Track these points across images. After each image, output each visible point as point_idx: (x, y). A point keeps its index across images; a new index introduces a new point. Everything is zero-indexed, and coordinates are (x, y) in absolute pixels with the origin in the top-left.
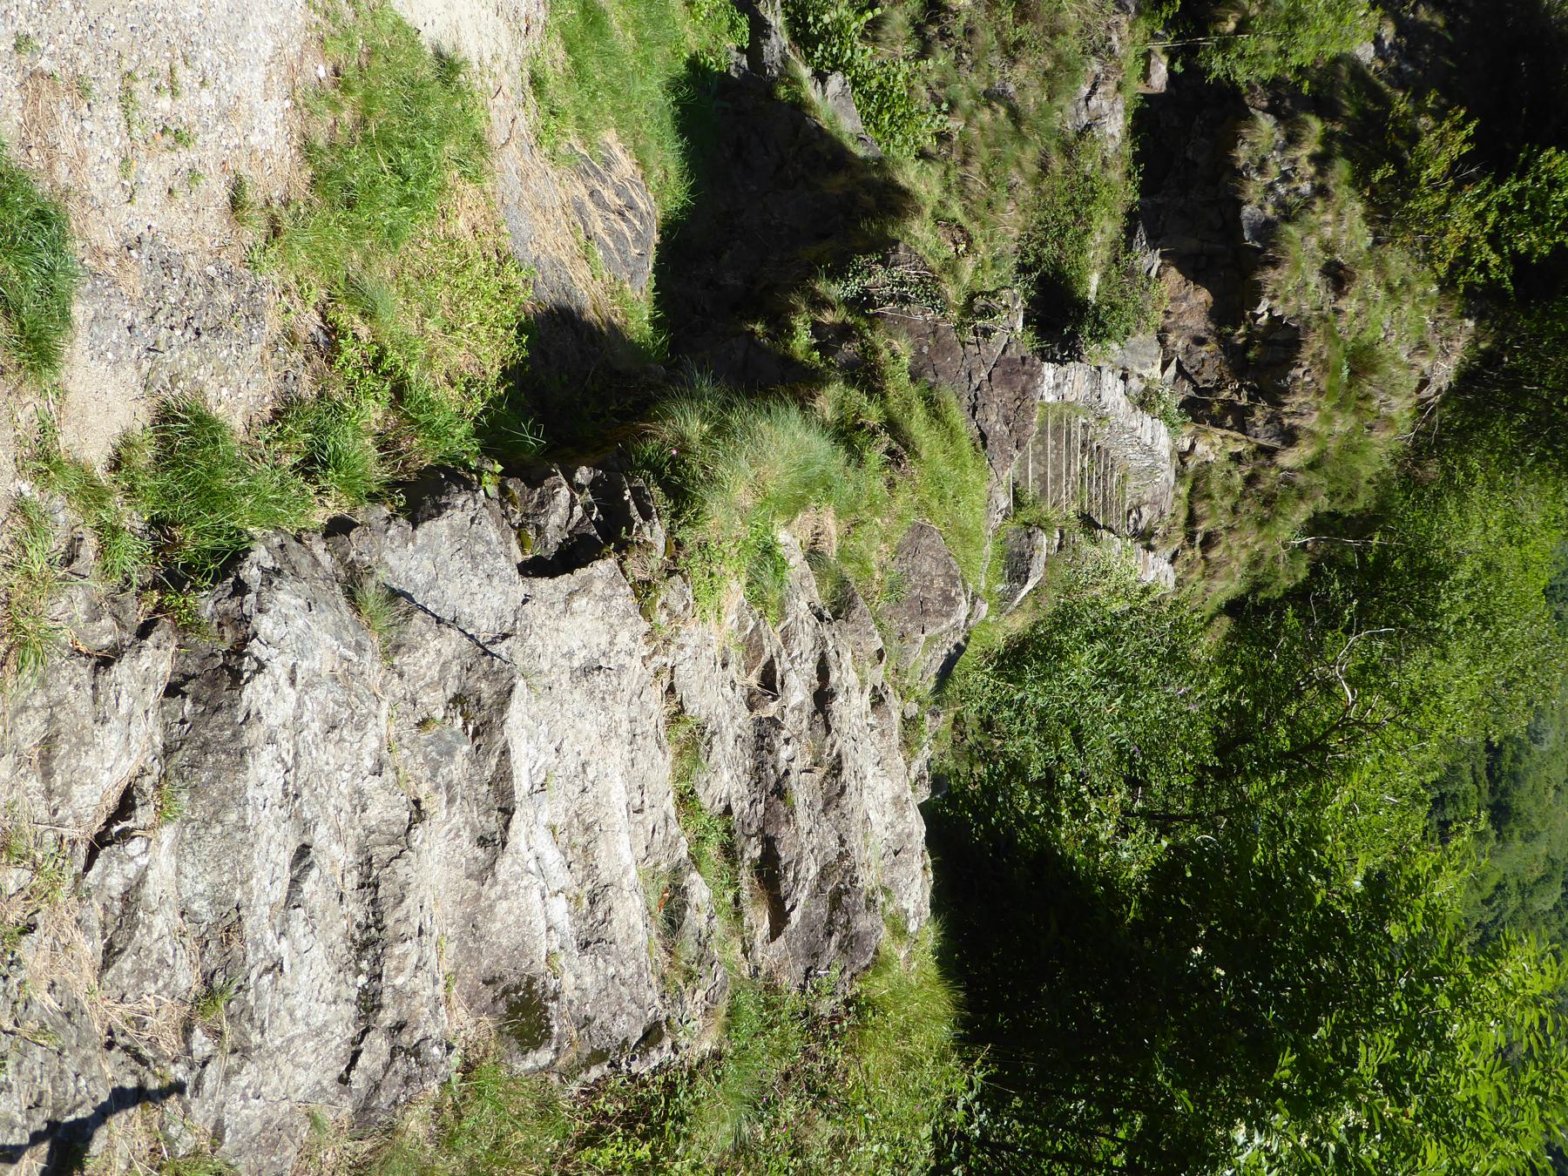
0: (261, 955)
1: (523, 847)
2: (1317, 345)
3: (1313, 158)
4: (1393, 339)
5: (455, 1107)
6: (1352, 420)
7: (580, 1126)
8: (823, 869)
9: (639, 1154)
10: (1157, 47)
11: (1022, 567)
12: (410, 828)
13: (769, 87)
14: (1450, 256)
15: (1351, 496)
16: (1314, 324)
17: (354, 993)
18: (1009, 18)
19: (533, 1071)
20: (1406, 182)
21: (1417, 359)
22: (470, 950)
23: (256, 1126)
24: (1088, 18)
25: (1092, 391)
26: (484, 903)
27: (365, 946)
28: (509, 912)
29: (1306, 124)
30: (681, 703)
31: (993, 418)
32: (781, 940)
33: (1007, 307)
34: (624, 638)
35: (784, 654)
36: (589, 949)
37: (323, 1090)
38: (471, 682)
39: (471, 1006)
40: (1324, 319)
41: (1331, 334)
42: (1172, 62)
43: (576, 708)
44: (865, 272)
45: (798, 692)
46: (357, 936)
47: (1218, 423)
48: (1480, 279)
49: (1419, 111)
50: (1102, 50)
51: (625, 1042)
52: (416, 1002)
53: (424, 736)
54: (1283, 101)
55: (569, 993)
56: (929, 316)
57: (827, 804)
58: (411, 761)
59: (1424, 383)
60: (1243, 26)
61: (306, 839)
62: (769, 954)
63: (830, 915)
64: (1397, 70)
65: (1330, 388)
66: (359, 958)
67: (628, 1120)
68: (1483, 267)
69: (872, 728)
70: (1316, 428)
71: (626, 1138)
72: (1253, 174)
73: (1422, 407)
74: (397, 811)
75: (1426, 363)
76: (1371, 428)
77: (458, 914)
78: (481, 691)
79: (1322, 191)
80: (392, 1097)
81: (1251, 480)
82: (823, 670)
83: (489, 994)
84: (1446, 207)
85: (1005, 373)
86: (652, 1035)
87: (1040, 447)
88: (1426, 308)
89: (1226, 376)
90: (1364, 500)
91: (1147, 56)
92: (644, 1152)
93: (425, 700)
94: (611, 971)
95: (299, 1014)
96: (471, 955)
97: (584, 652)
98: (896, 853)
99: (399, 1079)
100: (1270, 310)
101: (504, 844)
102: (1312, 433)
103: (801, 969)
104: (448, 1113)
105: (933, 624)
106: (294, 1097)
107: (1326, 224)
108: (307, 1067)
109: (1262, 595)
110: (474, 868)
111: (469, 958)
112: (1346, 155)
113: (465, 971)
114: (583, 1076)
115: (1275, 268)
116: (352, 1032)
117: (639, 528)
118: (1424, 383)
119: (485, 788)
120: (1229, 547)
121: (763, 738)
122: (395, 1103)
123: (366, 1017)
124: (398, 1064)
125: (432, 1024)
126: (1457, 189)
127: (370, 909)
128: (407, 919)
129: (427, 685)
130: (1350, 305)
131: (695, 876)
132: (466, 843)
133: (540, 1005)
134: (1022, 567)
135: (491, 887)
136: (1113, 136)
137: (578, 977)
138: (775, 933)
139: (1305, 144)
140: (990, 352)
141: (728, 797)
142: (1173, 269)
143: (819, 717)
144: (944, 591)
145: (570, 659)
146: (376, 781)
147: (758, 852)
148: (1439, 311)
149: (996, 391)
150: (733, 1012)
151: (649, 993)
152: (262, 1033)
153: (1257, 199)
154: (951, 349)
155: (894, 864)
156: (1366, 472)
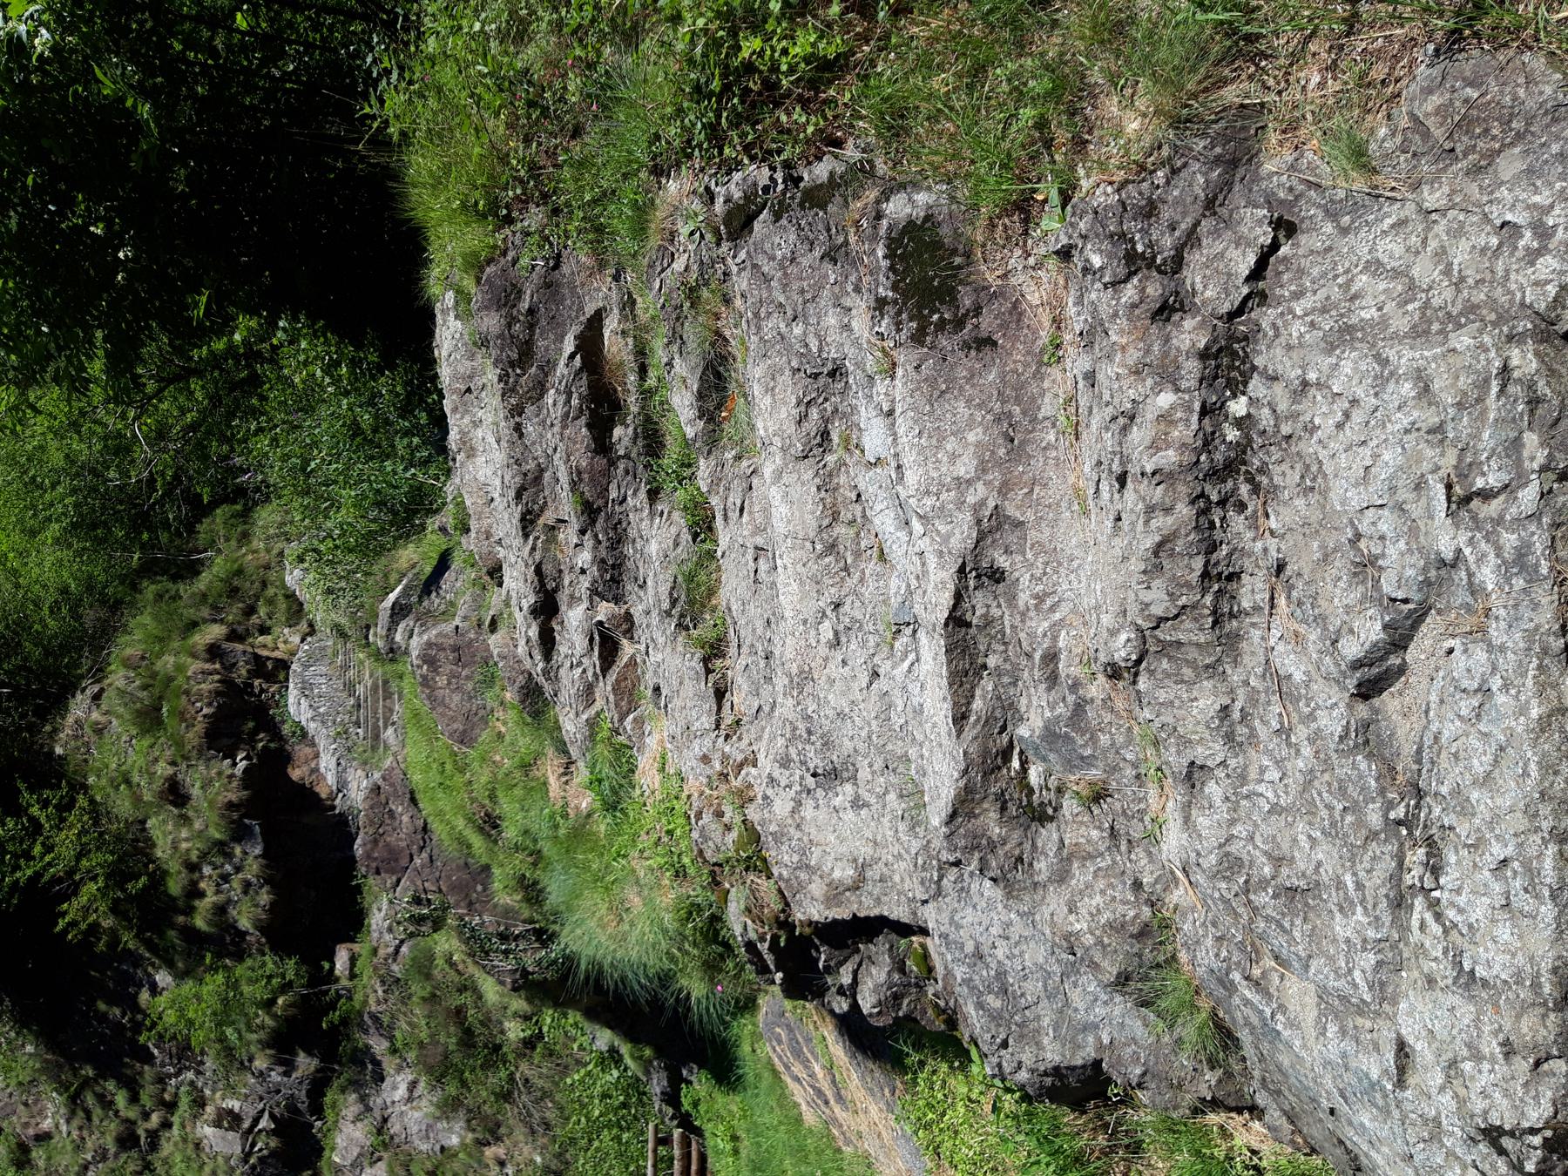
0: (1509, 539)
1: (932, 561)
2: (190, 735)
3: (202, 895)
4: (124, 738)
5: (1048, 144)
6: (159, 666)
7: (843, 93)
8: (541, 396)
9: (757, 43)
10: (344, 982)
12: (1139, 662)
13: (660, 1052)
14: (75, 812)
15: (159, 597)
17: (1256, 386)
18: (471, 1012)
19: (916, 186)
20: (118, 875)
21: (103, 719)
22: (1018, 400)
23: (1510, 165)
25: (345, 770)
26: (995, 476)
27: (1230, 468)
28: (954, 457)
29: (209, 923)
30: (708, 671)
31: (405, 819)
32: (590, 310)
33: (399, 923)
34: (782, 806)
35: (590, 673)
36: (830, 366)
37: (1332, 214)
38: (1016, 836)
39: (1015, 305)
40: (186, 758)
41: (179, 744)
43: (848, 728)
44: (545, 964)
45: (574, 619)
46: (1244, 489)
48: (46, 793)
49: (114, 935)
50: (391, 983)
51: (777, 217)
52: (1134, 355)
53: (1095, 773)
55: (861, 306)
56: (477, 920)
57: (538, 479)
58: (1120, 739)
59: (97, 697)
61: (1362, 710)
62: (600, 293)
63: (532, 335)
64: (136, 965)
65: (178, 697)
66: (1243, 447)
67: (772, 95)
68: (45, 804)
69: (499, 542)
70: (189, 660)
71: (775, 68)
72: (254, 880)
73: (99, 673)
74: (1162, 695)
75: (95, 716)
76: (143, 658)
77: (1038, 463)
78: (1000, 823)
79: (193, 867)
80: (1181, 181)
81: (251, 610)
82: (547, 642)
84: (79, 857)
85: (396, 860)
86: (739, 222)
88: (97, 764)
90: (150, 589)
91: (352, 976)
92: (750, 45)
93: (1095, 834)
94: (798, 330)
95: (1407, 389)
96: (1018, 392)
97: (837, 801)
98: (469, 390)
99: (1166, 214)
100: (235, 764)
101: (962, 570)
102: (194, 656)
103: (565, 269)
104: (1062, 135)
105: (446, 636)
106: (1410, 210)
107: (187, 840)
108: (1375, 267)
109: (238, 507)
110: (1012, 538)
111: (1020, 387)
112: (173, 899)
113: (1026, 365)
114: (840, 168)
116: (1266, 317)
117: (762, 939)
118: (97, 697)
119: (992, 661)
120: (268, 551)
121: (612, 579)
122: (1175, 172)
123: (1232, 338)
124: (1168, 242)
125: (1105, 311)
126: (70, 873)
127: (1218, 535)
128: (1150, 510)
129: (1091, 857)
130: (163, 769)
131: (690, 432)
132: (1025, 580)
133: (906, 296)
137: (847, 327)
138: (596, 321)
139: (209, 906)
140: (413, 882)
141: (652, 514)
142: (323, 796)
143: (551, 585)
144: (435, 670)
145: (857, 797)
146: (1200, 753)
147: (618, 432)
148: (86, 761)
149: (403, 844)
150: (640, 229)
151: (744, 286)
152: (1505, 369)
153: (250, 860)
155: (471, 377)
156: (146, 619)
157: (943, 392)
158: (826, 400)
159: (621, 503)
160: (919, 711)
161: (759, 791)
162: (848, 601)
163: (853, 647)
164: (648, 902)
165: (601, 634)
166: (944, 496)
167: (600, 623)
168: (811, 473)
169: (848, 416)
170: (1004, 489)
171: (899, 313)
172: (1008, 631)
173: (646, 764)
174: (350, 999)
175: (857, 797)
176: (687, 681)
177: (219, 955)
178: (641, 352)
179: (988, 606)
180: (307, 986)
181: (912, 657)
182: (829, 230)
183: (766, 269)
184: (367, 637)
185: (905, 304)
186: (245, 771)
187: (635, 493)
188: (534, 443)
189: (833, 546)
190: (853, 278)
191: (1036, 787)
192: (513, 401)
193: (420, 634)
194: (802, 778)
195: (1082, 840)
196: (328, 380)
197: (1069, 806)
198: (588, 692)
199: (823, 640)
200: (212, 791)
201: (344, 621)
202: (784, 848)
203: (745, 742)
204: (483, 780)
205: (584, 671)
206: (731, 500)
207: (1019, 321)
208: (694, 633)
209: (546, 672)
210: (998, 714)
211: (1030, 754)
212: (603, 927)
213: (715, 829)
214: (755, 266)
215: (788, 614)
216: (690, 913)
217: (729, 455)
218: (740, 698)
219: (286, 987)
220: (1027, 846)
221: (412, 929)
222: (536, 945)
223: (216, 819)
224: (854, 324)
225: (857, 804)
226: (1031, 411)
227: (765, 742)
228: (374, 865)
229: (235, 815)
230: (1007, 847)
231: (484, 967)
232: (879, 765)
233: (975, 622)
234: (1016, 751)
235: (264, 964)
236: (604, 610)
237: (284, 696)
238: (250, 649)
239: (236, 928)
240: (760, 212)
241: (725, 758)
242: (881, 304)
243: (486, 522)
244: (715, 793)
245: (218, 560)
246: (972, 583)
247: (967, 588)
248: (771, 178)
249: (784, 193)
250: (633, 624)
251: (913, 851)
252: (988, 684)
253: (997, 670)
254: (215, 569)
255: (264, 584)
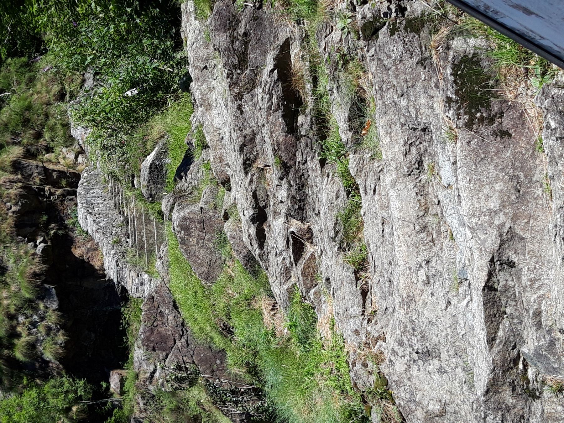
2: (4, 226)
3: (19, 336)
10: (117, 397)
11: (155, 174)
16: (8, 238)
22: (522, 169)
24: (158, 416)
25: (122, 269)
28: (488, 197)
29: (25, 355)
30: (357, 279)
31: (170, 318)
32: (281, 41)
33: (168, 381)
35: (288, 262)
36: (422, 126)
38: (521, 404)
39: (522, 114)
42: (108, 387)
44: (261, 410)
47: (62, 174)
50: (149, 398)
51: (392, 33)
54: (40, 366)
57: (253, 140)
60: (68, 410)
63: (246, 49)
72: (53, 326)
77: (532, 205)
78: (512, 396)
79: (12, 317)
81: (39, 135)
82: (261, 237)
83: (506, 123)
85: (165, 343)
87: (151, 242)
89: (59, 203)
91: (122, 393)
97: (430, 368)
98: (206, 67)
100: (36, 246)
101: (492, 260)
105: (195, 213)
107: (7, 298)
109: (24, 59)
110: (519, 246)
111: (523, 162)
113: (527, 150)
115: (34, 272)
119: (509, 310)
121: (300, 208)
131: (344, 138)
134: (155, 174)
135: (503, 225)
136: (139, 347)
137: (432, 107)
138: (286, 45)
139: (24, 344)
140: (176, 356)
143: (262, 204)
145: (441, 367)
147: (301, 119)
149: (170, 333)
153: (50, 312)
154: (201, 361)
155: (207, 60)
157: (482, 159)
158: (421, 143)
159: (304, 164)
160: (472, 329)
161: (387, 355)
162: (434, 259)
163: (437, 286)
164: (327, 404)
165: (294, 238)
166: (482, 218)
167: (293, 232)
168: (411, 186)
169: (433, 155)
170: (515, 218)
171: (459, 108)
172: (517, 295)
173: (323, 319)
174: (121, 408)
175: (441, 367)
176: (345, 283)
177: (32, 378)
178: (313, 69)
179: (507, 280)
180: (93, 399)
181: (468, 298)
182: (421, 48)
183: (386, 63)
184: (133, 183)
185: (462, 104)
186: (44, 251)
187: (312, 158)
188: (249, 118)
189: (425, 227)
190: (434, 80)
191: (531, 380)
192: (236, 91)
193: (179, 211)
194: (410, 353)
195: (553, 411)
196: (99, 9)
197: (547, 393)
198: (287, 272)
199: (420, 280)
200: (22, 264)
201: (117, 170)
202: (402, 390)
203: (379, 326)
204: (222, 304)
205: (284, 259)
206: (368, 183)
207: (523, 123)
208: (349, 254)
209: (261, 255)
210: (511, 339)
211: (529, 361)
212: (301, 413)
213: (362, 372)
214: (379, 59)
215: (401, 263)
216: (351, 415)
217: (368, 156)
218: (375, 296)
219: (78, 400)
220: (527, 410)
221: (176, 385)
222: (255, 398)
223: (26, 284)
224: (435, 106)
225: (441, 371)
226: (529, 176)
227: (389, 329)
228: (151, 345)
229: (39, 282)
230: (516, 410)
231: (222, 411)
232: (452, 352)
233: (499, 289)
234: (521, 359)
235: (62, 385)
236: (295, 225)
237: (75, 211)
238: (40, 164)
239: (43, 359)
240: (382, 27)
241: (368, 334)
242: (449, 100)
243: (219, 152)
244: (363, 353)
245: (13, 99)
246: (498, 268)
247: (495, 270)
248: (389, 8)
249: (396, 19)
250: (312, 234)
251: (471, 401)
252: (506, 323)
253: (512, 317)
254: (12, 105)
255: (47, 116)
